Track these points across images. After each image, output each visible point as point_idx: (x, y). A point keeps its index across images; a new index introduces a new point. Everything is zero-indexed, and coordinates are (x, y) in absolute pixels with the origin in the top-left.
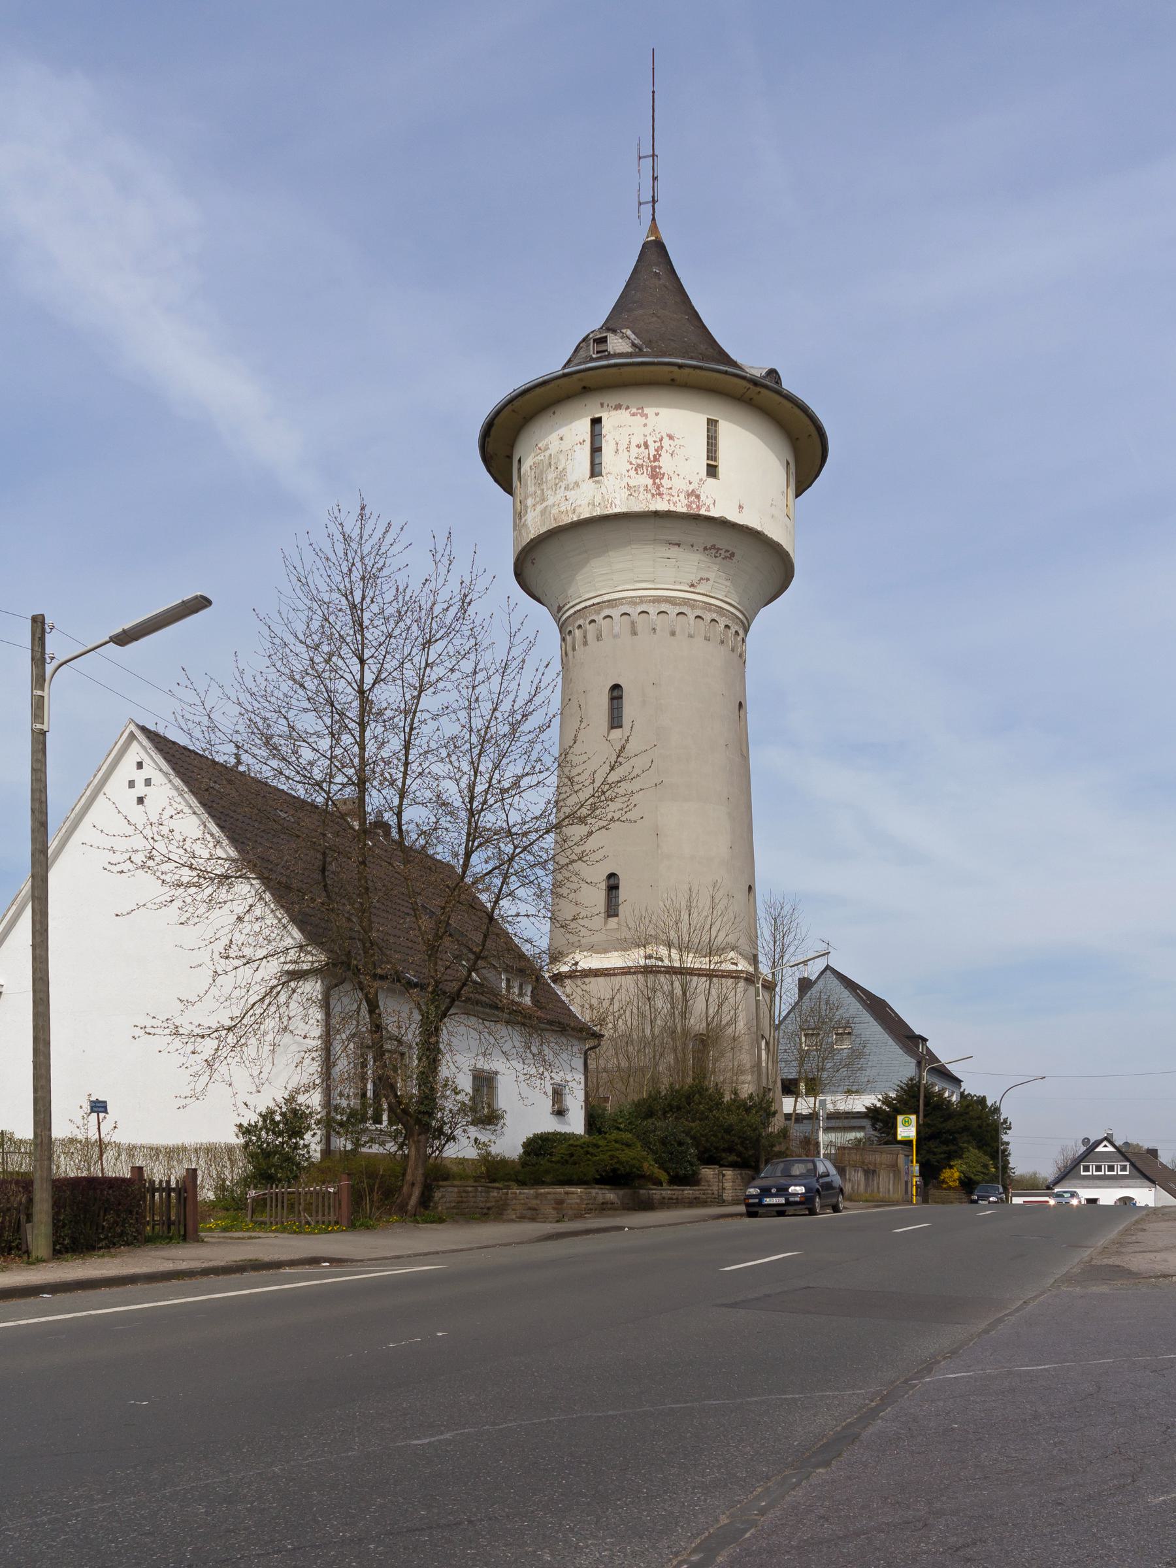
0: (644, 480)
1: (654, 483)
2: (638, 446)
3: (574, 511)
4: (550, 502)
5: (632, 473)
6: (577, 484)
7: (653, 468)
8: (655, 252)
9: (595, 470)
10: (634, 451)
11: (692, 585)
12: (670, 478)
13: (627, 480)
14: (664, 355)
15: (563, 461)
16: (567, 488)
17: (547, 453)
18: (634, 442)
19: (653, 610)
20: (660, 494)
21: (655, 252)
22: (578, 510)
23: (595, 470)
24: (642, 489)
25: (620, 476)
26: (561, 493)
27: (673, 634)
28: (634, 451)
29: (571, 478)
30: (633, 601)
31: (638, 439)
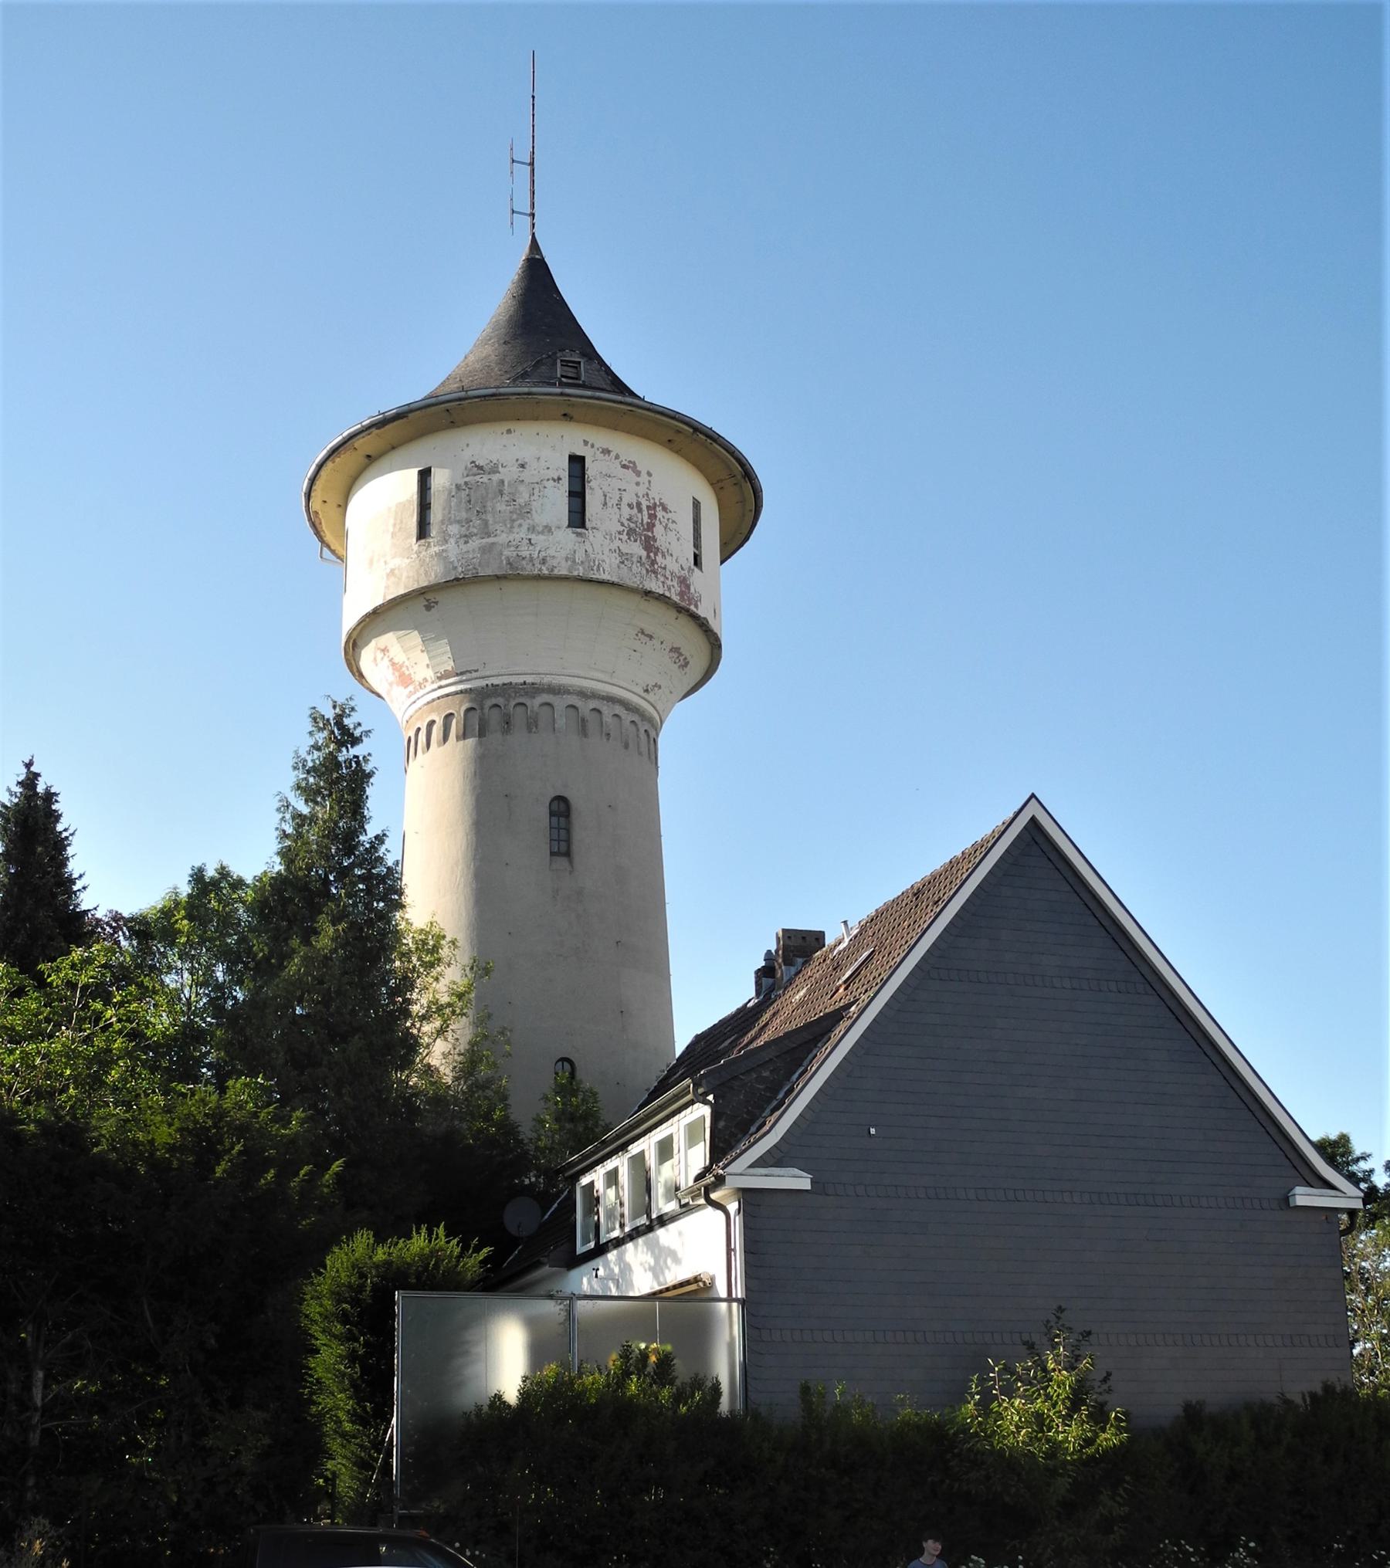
0: (637, 549)
1: (648, 557)
2: (630, 506)
3: (544, 561)
4: (502, 538)
5: (625, 537)
6: (548, 529)
7: (647, 538)
8: (537, 275)
9: (578, 518)
10: (626, 512)
11: (647, 691)
12: (663, 556)
13: (617, 543)
14: (610, 408)
15: (526, 496)
16: (532, 529)
17: (495, 478)
18: (625, 501)
19: (607, 710)
20: (655, 572)
21: (537, 275)
22: (550, 562)
23: (578, 518)
24: (635, 559)
25: (608, 535)
26: (522, 533)
27: (626, 746)
28: (626, 512)
29: (540, 519)
30: (583, 694)
31: (628, 498)
